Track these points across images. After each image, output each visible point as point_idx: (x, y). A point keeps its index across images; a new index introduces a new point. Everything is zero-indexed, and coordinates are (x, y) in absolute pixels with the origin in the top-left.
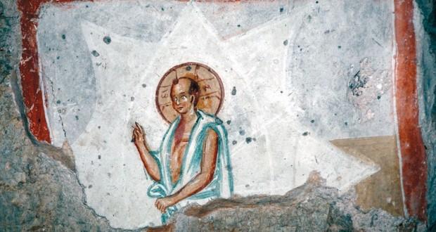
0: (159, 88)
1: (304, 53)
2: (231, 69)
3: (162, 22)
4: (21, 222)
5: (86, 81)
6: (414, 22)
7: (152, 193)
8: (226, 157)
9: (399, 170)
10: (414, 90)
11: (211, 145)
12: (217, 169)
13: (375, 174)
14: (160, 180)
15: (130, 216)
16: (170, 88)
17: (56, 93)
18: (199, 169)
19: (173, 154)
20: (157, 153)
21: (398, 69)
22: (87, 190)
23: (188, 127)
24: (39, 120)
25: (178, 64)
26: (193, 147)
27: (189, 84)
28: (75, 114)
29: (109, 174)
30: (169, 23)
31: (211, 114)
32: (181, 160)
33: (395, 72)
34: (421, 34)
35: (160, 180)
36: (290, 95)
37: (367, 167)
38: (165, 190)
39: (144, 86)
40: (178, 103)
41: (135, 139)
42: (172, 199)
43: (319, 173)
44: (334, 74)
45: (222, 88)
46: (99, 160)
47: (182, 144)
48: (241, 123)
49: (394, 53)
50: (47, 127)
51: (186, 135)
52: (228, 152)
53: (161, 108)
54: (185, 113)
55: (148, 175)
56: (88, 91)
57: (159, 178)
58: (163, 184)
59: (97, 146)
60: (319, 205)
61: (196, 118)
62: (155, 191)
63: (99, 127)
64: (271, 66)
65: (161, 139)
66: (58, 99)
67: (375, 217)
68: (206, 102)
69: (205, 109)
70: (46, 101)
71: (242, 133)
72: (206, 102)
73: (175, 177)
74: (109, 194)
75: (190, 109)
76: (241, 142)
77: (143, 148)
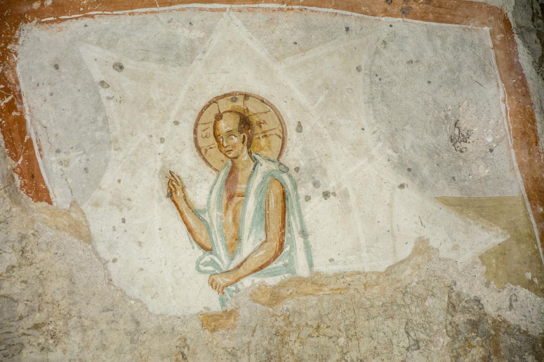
0: (196, 125)
1: (385, 84)
2: (292, 99)
3: (192, 41)
4: (17, 318)
5: (94, 121)
6: (520, 61)
7: (202, 268)
8: (297, 219)
9: (535, 239)
10: (537, 143)
11: (276, 203)
12: (287, 235)
13: (505, 242)
14: (211, 250)
15: (174, 298)
16: (211, 125)
17: (53, 140)
18: (262, 235)
19: (225, 213)
20: (204, 212)
21: (511, 116)
22: (111, 267)
23: (242, 176)
24: (33, 176)
25: (220, 95)
26: (251, 204)
27: (238, 119)
28: (83, 165)
29: (140, 244)
30: (202, 41)
31: (272, 159)
32: (237, 222)
33: (507, 119)
34: (532, 76)
35: (211, 250)
36: (374, 132)
37: (492, 233)
38: (220, 263)
39: (176, 123)
40: (225, 145)
41: (171, 192)
42: (232, 276)
43: (428, 240)
44: (427, 114)
45: (282, 123)
46: (123, 225)
47: (236, 199)
48: (313, 171)
49: (502, 96)
50: (44, 184)
51: (241, 188)
52: (300, 211)
53: (203, 151)
54: (236, 158)
55: (194, 242)
56: (97, 134)
57: (209, 246)
58: (216, 255)
59: (118, 206)
60: (433, 287)
61: (253, 165)
62: (206, 264)
63: (119, 181)
64: (344, 96)
65: (208, 193)
66: (57, 147)
67: (514, 298)
68: (263, 142)
69: (263, 152)
70: (40, 150)
71: (316, 184)
72: (263, 142)
73: (232, 245)
74: (142, 270)
75: (242, 152)
76: (317, 200)
77: (183, 206)
